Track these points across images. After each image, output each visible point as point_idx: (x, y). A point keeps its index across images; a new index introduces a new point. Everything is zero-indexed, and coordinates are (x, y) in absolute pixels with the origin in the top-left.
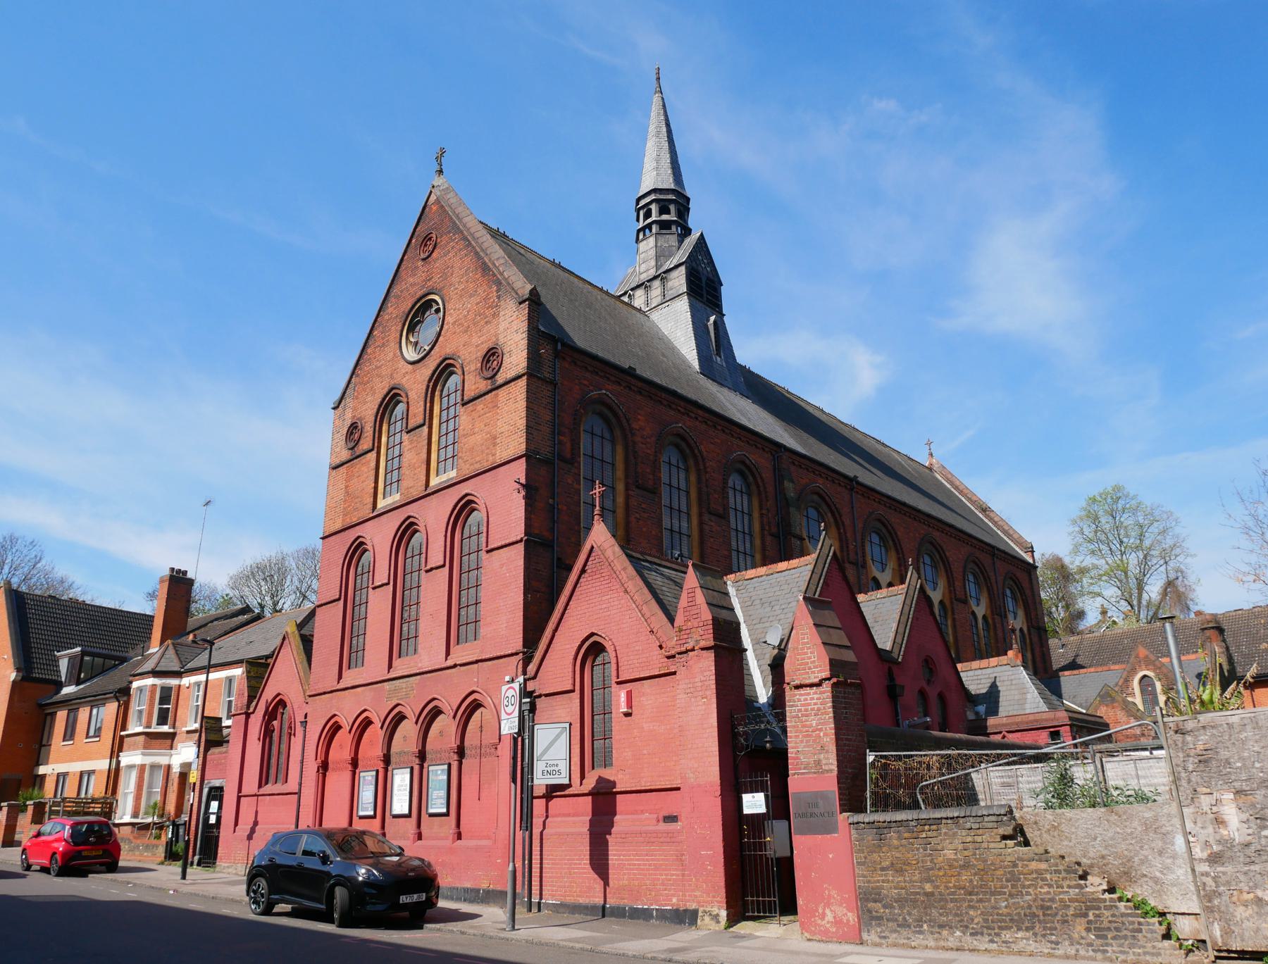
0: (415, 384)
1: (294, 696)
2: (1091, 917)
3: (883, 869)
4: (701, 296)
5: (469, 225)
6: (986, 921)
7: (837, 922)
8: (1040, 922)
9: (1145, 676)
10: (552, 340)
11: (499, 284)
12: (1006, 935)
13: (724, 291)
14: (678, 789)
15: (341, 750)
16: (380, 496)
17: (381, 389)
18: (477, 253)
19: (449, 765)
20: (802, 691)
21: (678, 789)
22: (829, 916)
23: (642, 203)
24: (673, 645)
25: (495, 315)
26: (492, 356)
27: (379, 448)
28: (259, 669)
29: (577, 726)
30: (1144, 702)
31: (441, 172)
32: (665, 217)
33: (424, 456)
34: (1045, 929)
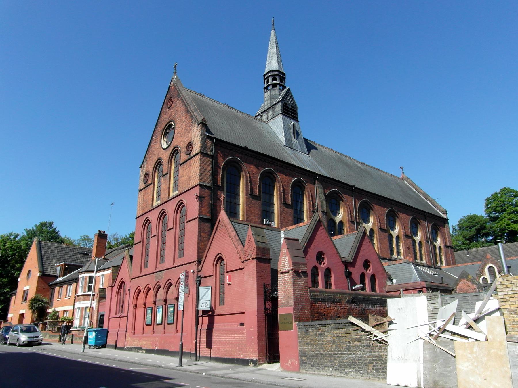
0: (165, 157)
1: (127, 280)
2: (374, 364)
3: (307, 344)
4: (289, 114)
5: (183, 94)
6: (340, 364)
7: (292, 363)
8: (357, 365)
9: (490, 267)
10: (211, 139)
11: (192, 116)
12: (346, 370)
13: (299, 112)
14: (244, 313)
15: (141, 300)
16: (155, 201)
17: (155, 159)
18: (185, 105)
19: (174, 305)
20: (283, 275)
21: (244, 313)
22: (290, 362)
23: (266, 77)
24: (244, 258)
25: (191, 130)
26: (190, 145)
27: (154, 183)
28: (116, 269)
29: (214, 289)
30: (491, 278)
31: (176, 72)
32: (274, 82)
33: (168, 185)
34: (359, 368)
